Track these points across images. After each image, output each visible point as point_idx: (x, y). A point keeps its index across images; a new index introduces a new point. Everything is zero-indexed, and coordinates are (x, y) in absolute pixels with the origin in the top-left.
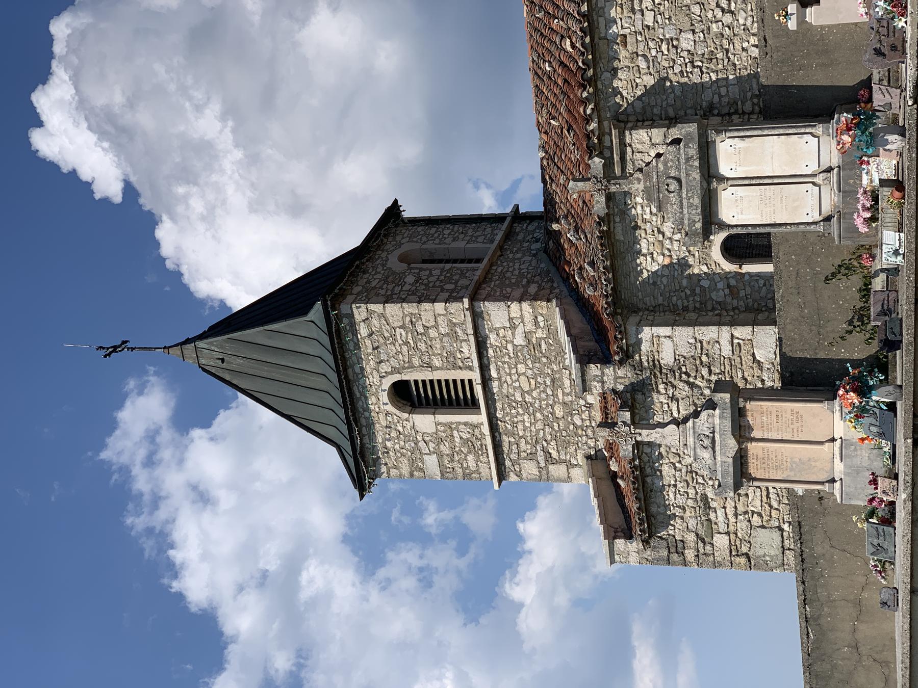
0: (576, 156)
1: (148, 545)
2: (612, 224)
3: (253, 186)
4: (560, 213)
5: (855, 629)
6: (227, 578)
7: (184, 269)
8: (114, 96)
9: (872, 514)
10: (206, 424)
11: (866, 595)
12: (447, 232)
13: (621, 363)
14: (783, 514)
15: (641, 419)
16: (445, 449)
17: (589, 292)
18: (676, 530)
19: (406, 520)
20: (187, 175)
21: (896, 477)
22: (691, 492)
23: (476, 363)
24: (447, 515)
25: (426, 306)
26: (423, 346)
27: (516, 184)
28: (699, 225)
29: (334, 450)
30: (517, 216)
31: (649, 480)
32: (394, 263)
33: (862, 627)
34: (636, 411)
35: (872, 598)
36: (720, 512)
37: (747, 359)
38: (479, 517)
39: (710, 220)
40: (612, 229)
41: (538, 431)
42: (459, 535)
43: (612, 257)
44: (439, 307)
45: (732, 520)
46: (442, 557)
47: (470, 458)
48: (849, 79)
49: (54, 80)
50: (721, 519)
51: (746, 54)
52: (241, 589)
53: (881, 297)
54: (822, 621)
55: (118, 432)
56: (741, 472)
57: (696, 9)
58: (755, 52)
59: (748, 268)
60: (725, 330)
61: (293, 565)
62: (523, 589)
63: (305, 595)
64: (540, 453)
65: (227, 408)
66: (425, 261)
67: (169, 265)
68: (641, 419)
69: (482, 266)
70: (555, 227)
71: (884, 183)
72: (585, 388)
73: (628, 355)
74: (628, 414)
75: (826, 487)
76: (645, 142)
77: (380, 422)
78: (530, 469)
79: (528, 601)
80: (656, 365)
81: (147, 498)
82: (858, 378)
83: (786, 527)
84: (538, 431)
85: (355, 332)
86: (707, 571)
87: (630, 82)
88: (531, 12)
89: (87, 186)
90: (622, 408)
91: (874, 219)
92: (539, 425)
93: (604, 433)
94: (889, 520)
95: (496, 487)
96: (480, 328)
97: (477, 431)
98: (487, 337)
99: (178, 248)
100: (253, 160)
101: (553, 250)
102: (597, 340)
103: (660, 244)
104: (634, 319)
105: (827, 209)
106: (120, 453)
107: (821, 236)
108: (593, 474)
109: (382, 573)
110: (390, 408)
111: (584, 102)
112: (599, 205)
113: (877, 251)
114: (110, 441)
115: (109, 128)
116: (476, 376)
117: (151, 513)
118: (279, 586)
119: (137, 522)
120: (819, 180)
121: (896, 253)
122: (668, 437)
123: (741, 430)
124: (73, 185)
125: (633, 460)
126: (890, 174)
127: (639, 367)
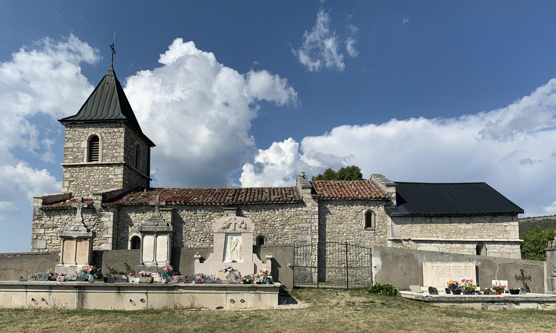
0: (165, 198)
1: (38, 43)
3: (159, 103)
4: (149, 192)
5: (12, 269)
6: (25, 68)
7: (136, 77)
8: (188, 66)
9: (52, 274)
10: (82, 72)
11: (24, 272)
13: (102, 206)
14: (51, 249)
15: (84, 210)
16: (75, 150)
17: (125, 198)
18: (45, 218)
19: (47, 133)
20: (164, 84)
21: (64, 281)
22: (59, 223)
24: (49, 147)
25: (123, 150)
26: (110, 147)
27: (156, 180)
28: (144, 230)
30: (149, 180)
32: (137, 142)
33: (13, 271)
35: (23, 274)
36: (52, 231)
37: (102, 242)
38: (47, 157)
39: (144, 233)
42: (41, 150)
43: (135, 206)
44: (123, 154)
45: (49, 235)
46: (33, 144)
47: (72, 157)
48: (181, 270)
49: (196, 50)
50: (49, 232)
51: (188, 244)
52: (21, 72)
53: (120, 277)
54: (15, 260)
55: (80, 42)
56: (66, 238)
57: (201, 232)
58: (189, 247)
59: (129, 243)
60: (111, 236)
61: (30, 92)
62: (21, 169)
63: (20, 94)
64: (73, 179)
65: (88, 81)
66: (137, 152)
67: (138, 72)
68: (84, 210)
69: (135, 168)
70: (145, 190)
71: (153, 278)
72: (94, 195)
73: (105, 208)
74: (86, 206)
75: (61, 262)
76: (168, 216)
77: (85, 131)
78: (67, 175)
79: (16, 169)
80: (101, 216)
81: (56, 46)
82: (96, 271)
83: (47, 250)
85: (115, 127)
86: (31, 227)
87: (184, 214)
88: (205, 190)
89: (164, 53)
90: (88, 205)
91: (143, 275)
92: (82, 180)
93: (80, 199)
94: (50, 279)
98: (112, 167)
99: (143, 76)
100: (167, 105)
101: (138, 189)
102: (109, 199)
103: (138, 219)
104: (116, 210)
105: (146, 264)
106: (72, 41)
107: (139, 262)
108: (65, 194)
109: (27, 123)
110: (90, 134)
111: (180, 201)
112: (152, 203)
113: (133, 276)
114: (77, 38)
115: (180, 63)
116: (99, 162)
117: (50, 47)
118: (22, 86)
119: (47, 41)
120: (154, 262)
121: (133, 281)
122: (78, 217)
123: (80, 239)
124: (165, 49)
125: (70, 207)
126: (155, 280)
127: (100, 211)
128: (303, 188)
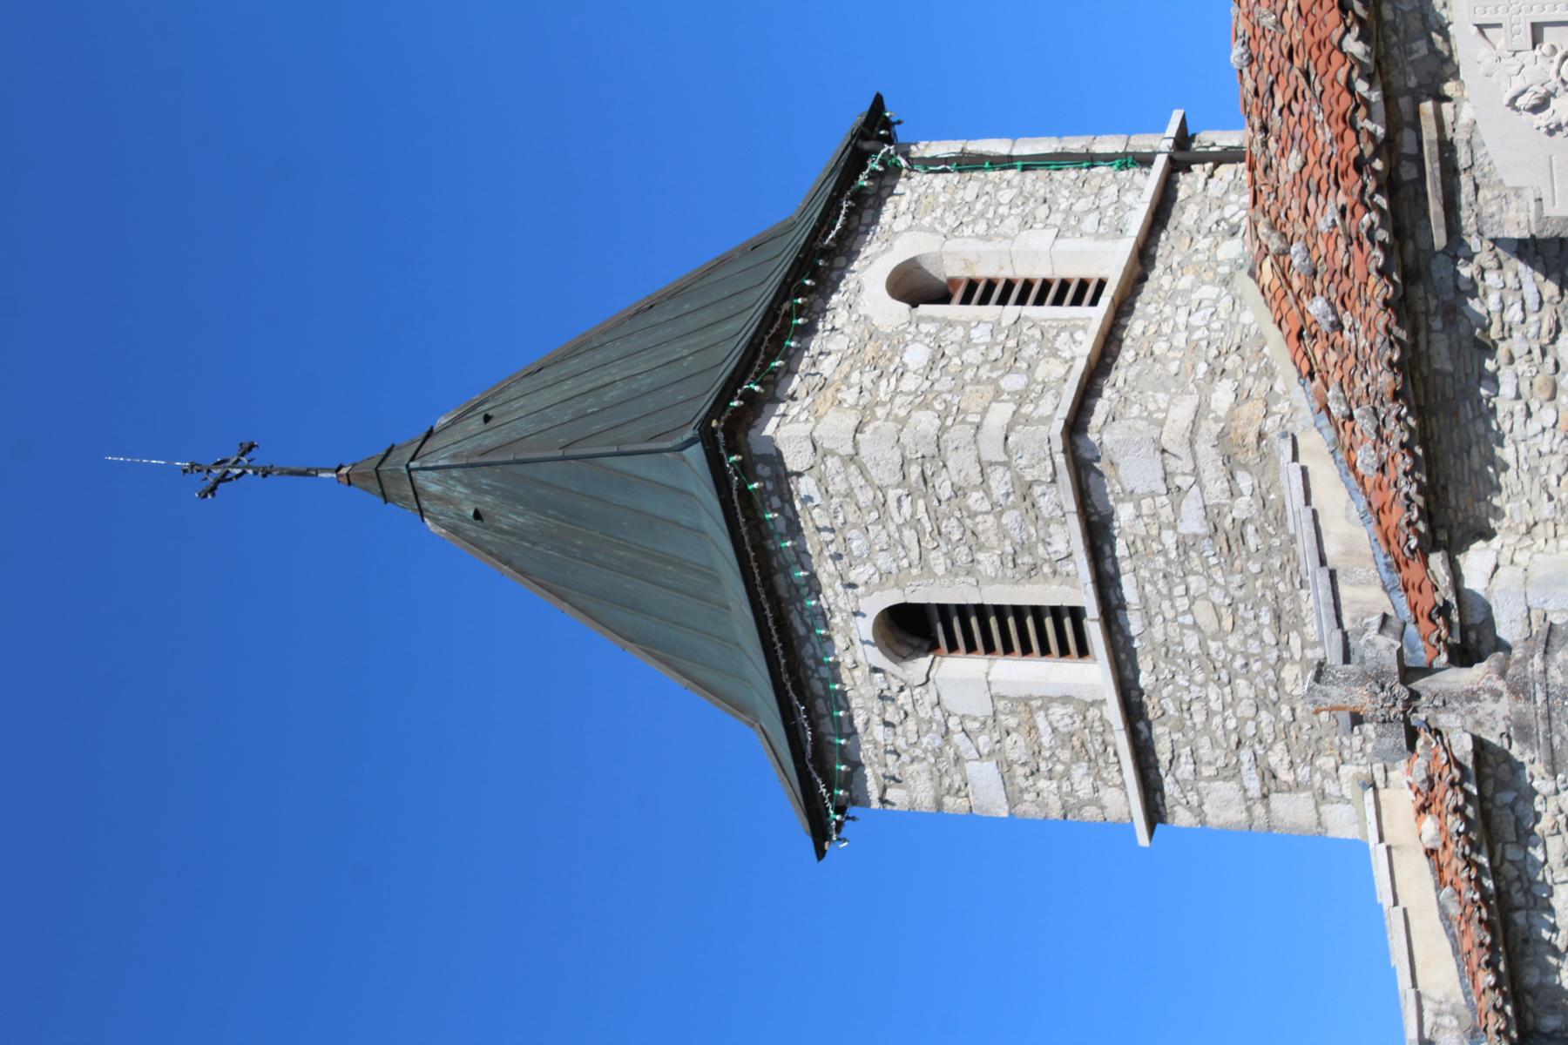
2: (1422, 335)
12: (1006, 196)
16: (1016, 746)
29: (787, 430)
31: (1519, 918)
34: (1488, 771)
40: (1422, 346)
41: (1242, 722)
84: (1242, 722)
92: (1245, 709)
95: (1143, 839)
97: (1093, 713)
110: (876, 656)
116: (1087, 599)
128: (1103, 701)
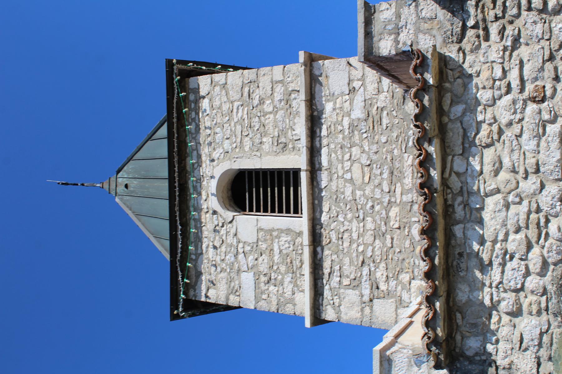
23: (303, 142)
31: (458, 230)
44: (278, 70)
77: (208, 222)
92: (368, 238)
96: (317, 96)
